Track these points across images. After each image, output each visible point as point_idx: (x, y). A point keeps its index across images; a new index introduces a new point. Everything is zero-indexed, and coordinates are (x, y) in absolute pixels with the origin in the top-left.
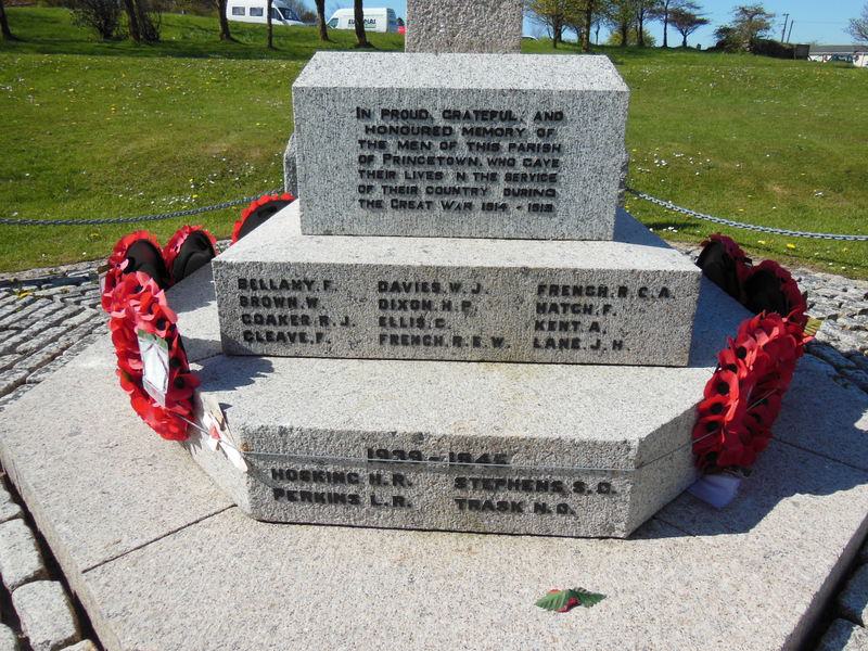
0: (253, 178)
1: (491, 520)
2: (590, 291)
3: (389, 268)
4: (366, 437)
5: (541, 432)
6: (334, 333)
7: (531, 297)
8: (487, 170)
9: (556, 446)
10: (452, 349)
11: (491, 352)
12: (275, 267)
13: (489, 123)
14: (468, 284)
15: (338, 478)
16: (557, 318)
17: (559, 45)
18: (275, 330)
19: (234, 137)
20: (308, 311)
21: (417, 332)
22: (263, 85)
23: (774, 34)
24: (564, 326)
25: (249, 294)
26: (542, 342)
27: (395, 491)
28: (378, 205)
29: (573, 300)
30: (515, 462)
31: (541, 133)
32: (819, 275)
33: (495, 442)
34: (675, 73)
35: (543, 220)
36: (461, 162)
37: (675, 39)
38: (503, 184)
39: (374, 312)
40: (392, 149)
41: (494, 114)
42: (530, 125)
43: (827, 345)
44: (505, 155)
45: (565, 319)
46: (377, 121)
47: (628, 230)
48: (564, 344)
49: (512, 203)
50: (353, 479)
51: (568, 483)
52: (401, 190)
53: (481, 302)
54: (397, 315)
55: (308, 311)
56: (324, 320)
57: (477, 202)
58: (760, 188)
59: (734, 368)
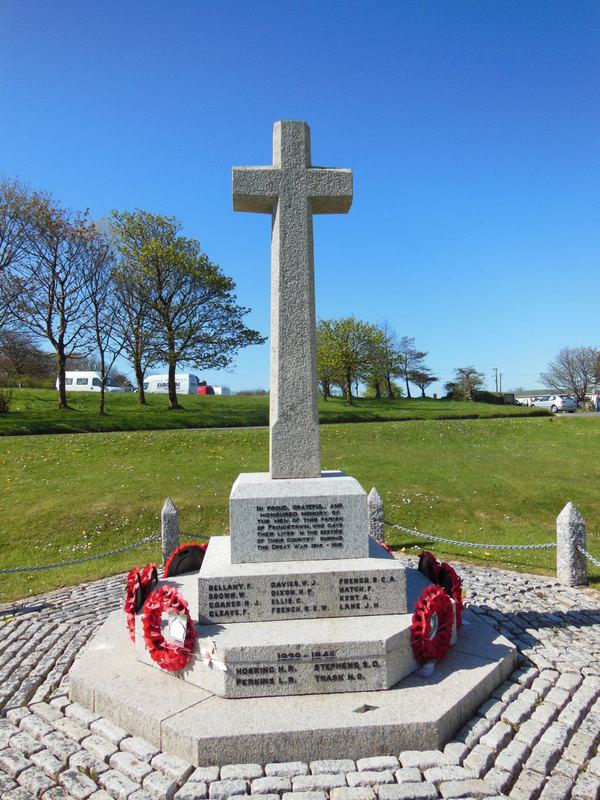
0: (128, 527)
1: (330, 686)
2: (361, 580)
3: (275, 577)
4: (277, 648)
5: (348, 640)
6: (251, 609)
7: (337, 585)
8: (313, 529)
9: (353, 645)
10: (305, 613)
11: (322, 613)
12: (226, 579)
13: (312, 510)
14: (310, 581)
15: (265, 670)
16: (349, 594)
17: (328, 399)
18: (224, 610)
19: (109, 497)
20: (240, 599)
21: (289, 606)
22: (115, 453)
23: (489, 386)
24: (352, 598)
25: (213, 593)
26: (344, 607)
27: (289, 675)
28: (266, 548)
29: (354, 585)
30: (339, 654)
31: (334, 513)
32: (503, 572)
33: (330, 645)
34: (415, 428)
35: (339, 550)
36: (301, 527)
37: (416, 392)
38: (320, 535)
39: (269, 597)
40: (272, 523)
41: (314, 506)
42: (329, 510)
43: (497, 610)
44: (319, 523)
45: (352, 594)
46: (265, 511)
47: (376, 551)
48: (353, 606)
49: (325, 543)
50: (272, 670)
51: (361, 663)
52: (276, 541)
53: (316, 589)
54: (279, 598)
55: (240, 599)
56: (247, 603)
57: (309, 544)
58: (472, 514)
59: (422, 609)
